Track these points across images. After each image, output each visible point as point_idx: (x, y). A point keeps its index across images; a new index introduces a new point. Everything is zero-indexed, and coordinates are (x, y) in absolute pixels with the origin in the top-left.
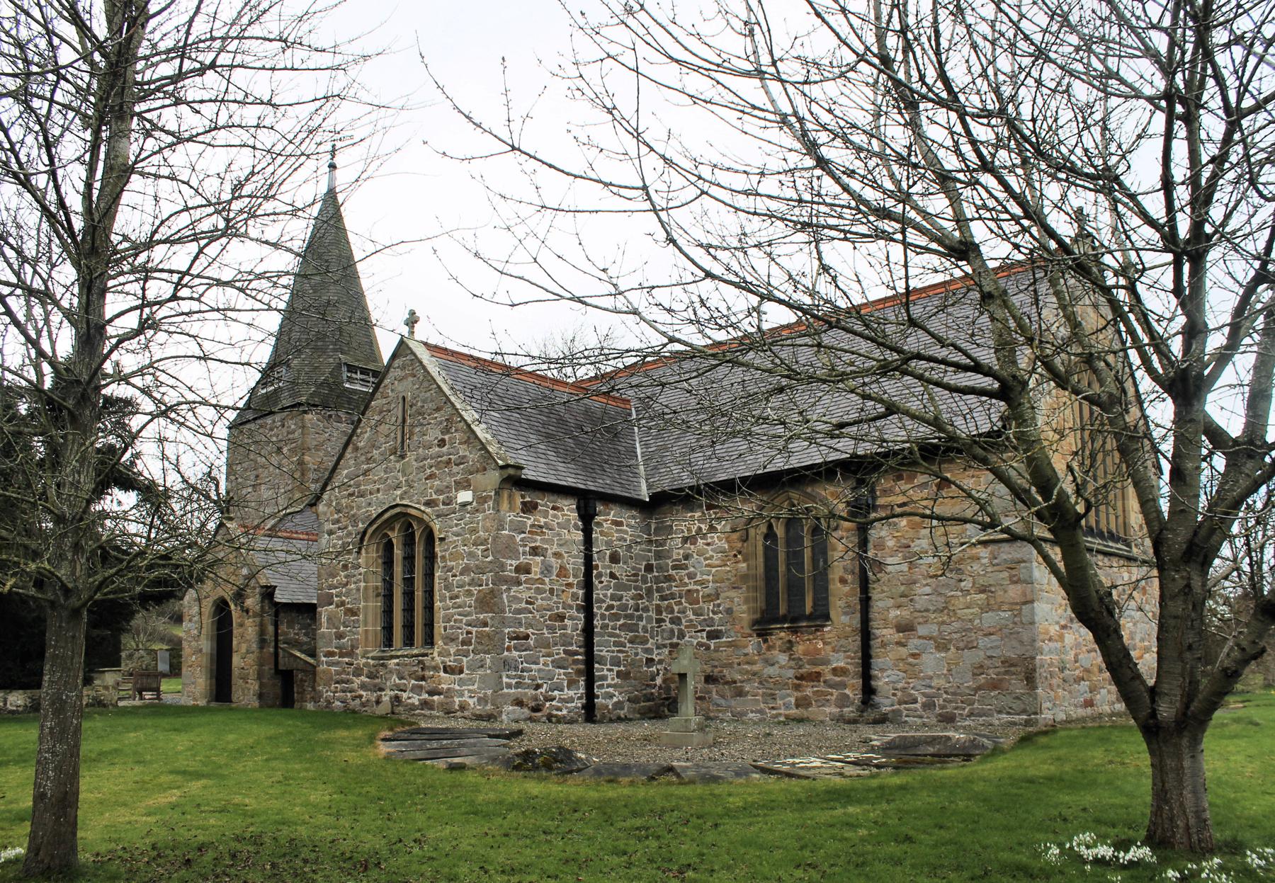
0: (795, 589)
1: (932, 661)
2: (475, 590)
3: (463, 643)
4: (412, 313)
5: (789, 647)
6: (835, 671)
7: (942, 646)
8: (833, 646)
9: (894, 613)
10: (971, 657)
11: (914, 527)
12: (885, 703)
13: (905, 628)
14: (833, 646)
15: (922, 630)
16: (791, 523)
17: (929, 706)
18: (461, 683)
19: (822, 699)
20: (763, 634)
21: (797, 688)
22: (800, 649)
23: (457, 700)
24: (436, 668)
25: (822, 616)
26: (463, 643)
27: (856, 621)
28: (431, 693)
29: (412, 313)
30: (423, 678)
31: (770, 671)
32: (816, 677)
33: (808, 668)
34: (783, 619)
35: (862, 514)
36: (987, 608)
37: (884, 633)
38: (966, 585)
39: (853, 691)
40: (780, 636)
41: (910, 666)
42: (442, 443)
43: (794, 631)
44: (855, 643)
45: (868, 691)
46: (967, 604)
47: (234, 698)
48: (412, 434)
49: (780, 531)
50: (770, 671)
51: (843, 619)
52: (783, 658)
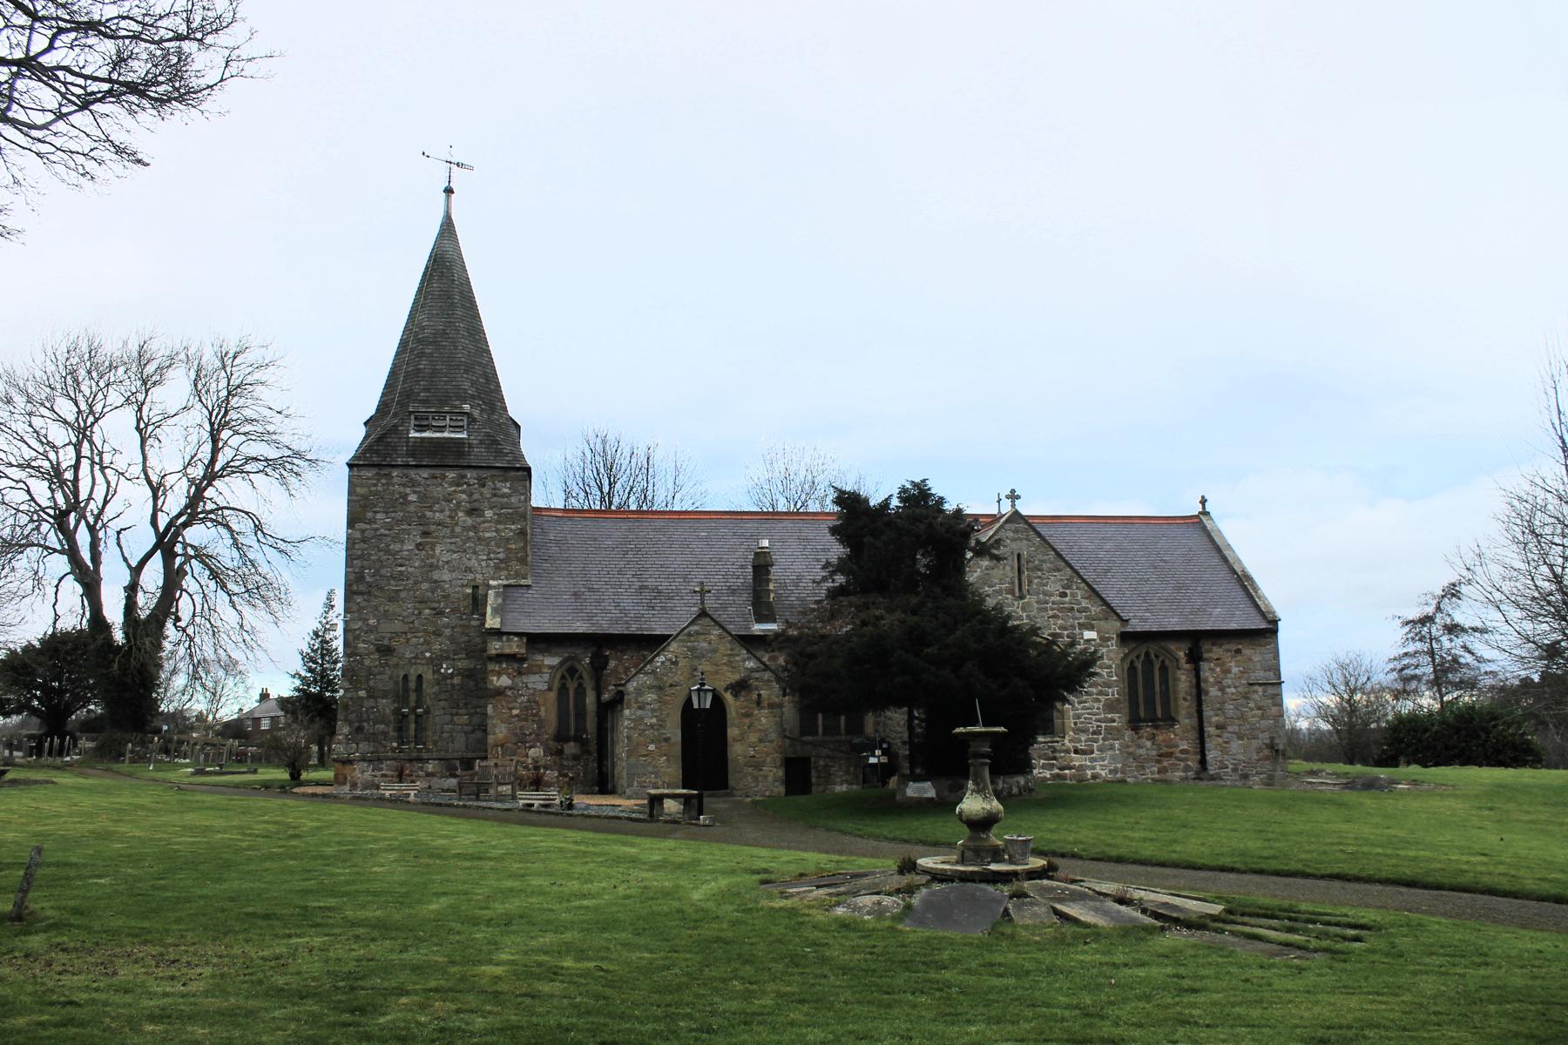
0: (1150, 703)
1: (1236, 746)
2: (1102, 698)
3: (1094, 733)
4: (1013, 491)
5: (1152, 738)
6: (1182, 752)
7: (1241, 737)
8: (1181, 738)
9: (1215, 719)
10: (1255, 743)
11: (721, 637)
12: (1212, 770)
13: (1220, 727)
14: (1181, 738)
15: (1230, 729)
16: (1148, 662)
17: (1235, 770)
18: (1093, 760)
19: (1174, 767)
20: (1136, 729)
21: (1159, 762)
22: (1160, 738)
23: (1089, 773)
24: (1068, 751)
25: (1170, 720)
26: (1094, 733)
27: (1195, 722)
28: (1061, 769)
29: (1013, 491)
30: (1055, 758)
31: (1142, 751)
32: (1170, 755)
33: (1165, 750)
34: (1144, 721)
35: (1195, 658)
36: (1263, 717)
37: (1210, 730)
38: (1252, 705)
39: (1193, 763)
40: (1147, 730)
41: (1224, 750)
42: (1064, 595)
43: (1156, 727)
44: (1194, 735)
45: (1203, 762)
46: (1253, 716)
47: (731, 782)
48: (1030, 582)
49: (1139, 666)
50: (1142, 751)
51: (1185, 721)
52: (1149, 744)
